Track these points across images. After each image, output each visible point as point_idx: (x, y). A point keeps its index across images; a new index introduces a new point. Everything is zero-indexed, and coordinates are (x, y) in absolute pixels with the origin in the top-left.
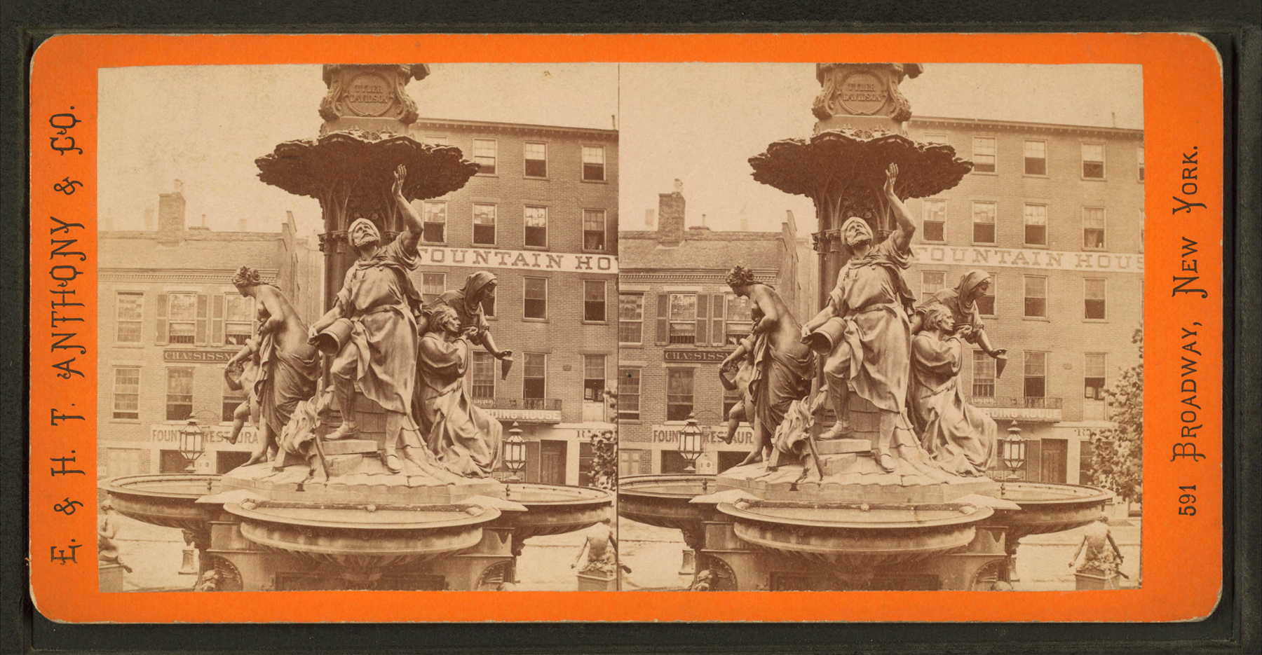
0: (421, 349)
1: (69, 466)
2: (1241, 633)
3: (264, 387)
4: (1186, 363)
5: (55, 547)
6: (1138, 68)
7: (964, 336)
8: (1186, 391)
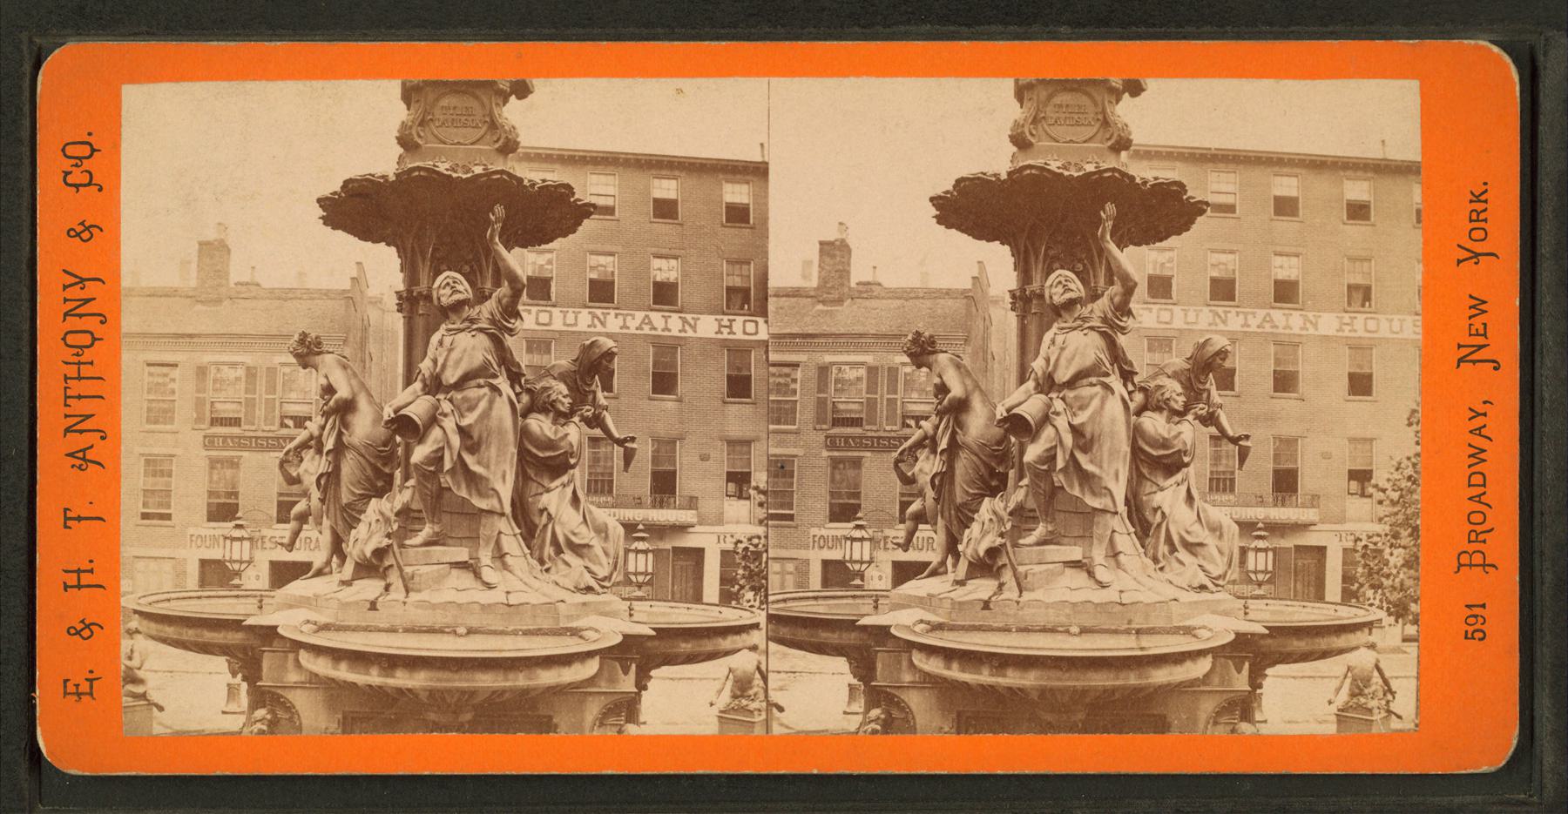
0: (524, 434)
1: (86, 579)
2: (1542, 787)
3: (327, 481)
4: (1472, 451)
5: (68, 680)
6: (1414, 85)
7: (1197, 417)
8: (1474, 485)
